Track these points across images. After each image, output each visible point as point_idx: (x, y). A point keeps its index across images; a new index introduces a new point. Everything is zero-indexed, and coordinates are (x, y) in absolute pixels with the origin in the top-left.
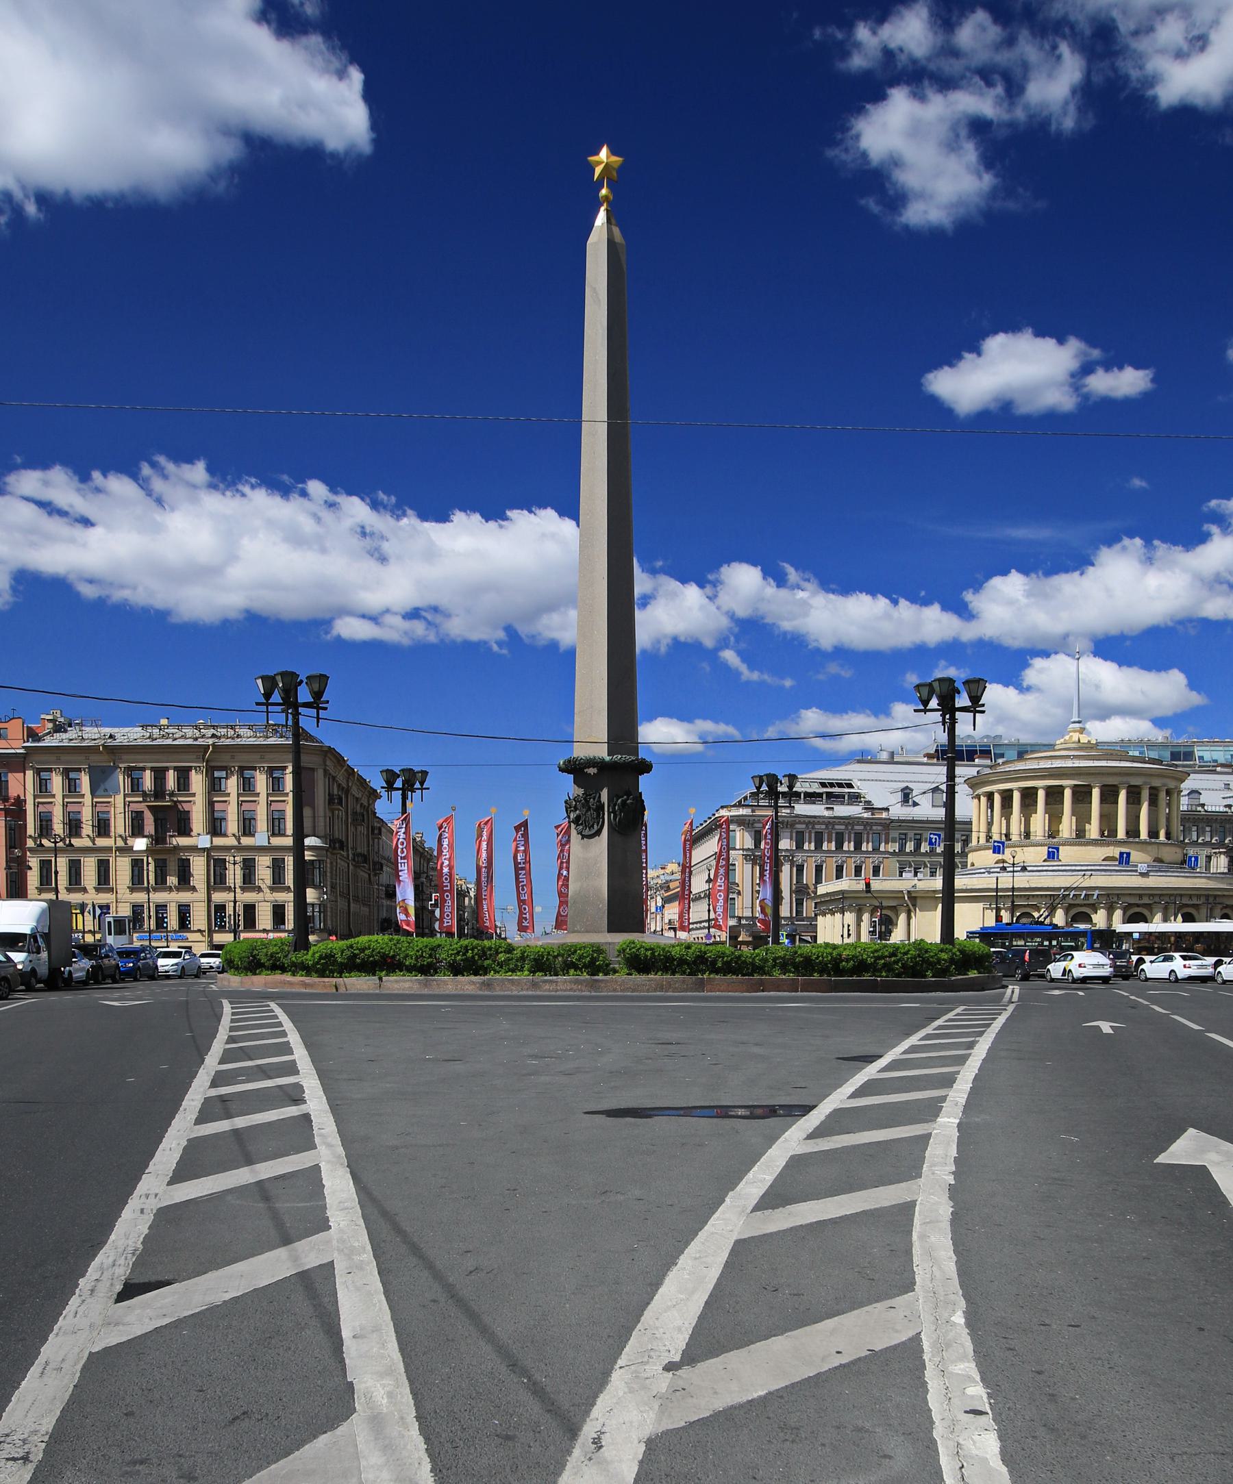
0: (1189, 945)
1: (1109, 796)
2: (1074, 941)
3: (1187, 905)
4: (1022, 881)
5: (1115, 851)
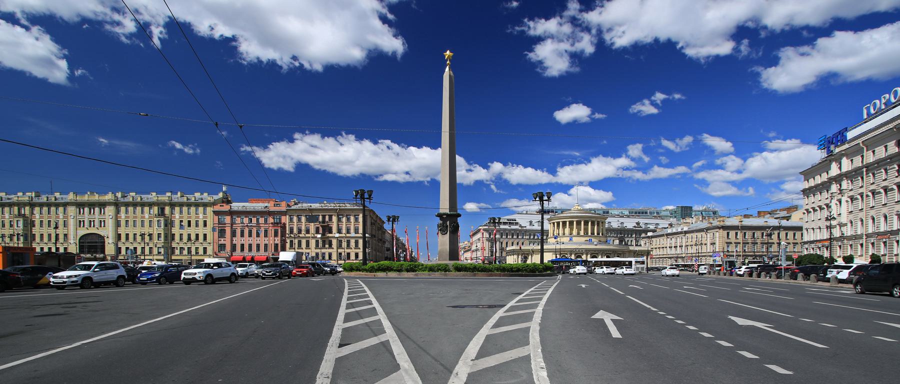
0: (608, 264)
1: (586, 223)
2: (577, 263)
3: (608, 253)
4: (563, 247)
5: (588, 239)
